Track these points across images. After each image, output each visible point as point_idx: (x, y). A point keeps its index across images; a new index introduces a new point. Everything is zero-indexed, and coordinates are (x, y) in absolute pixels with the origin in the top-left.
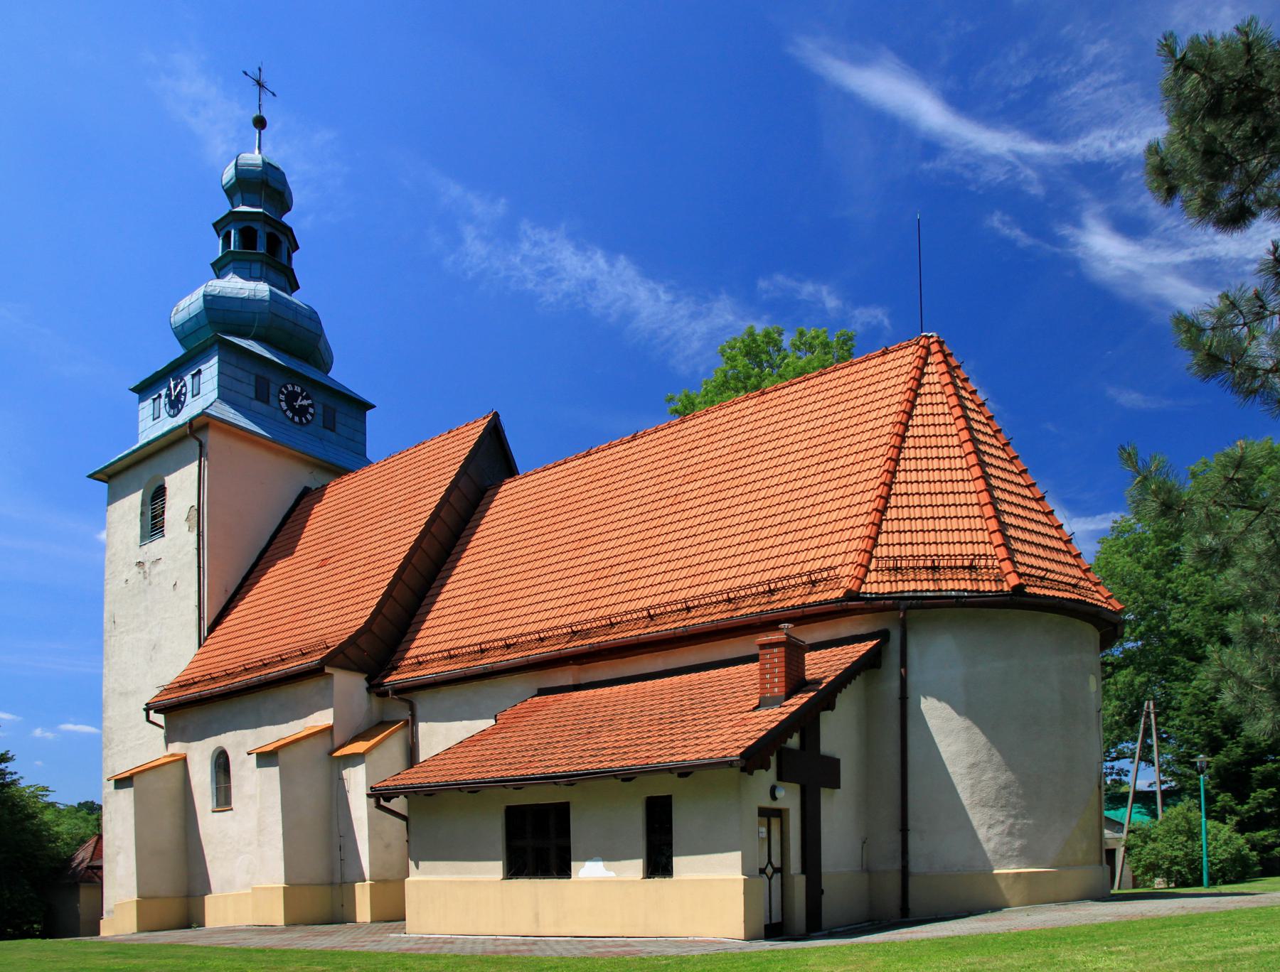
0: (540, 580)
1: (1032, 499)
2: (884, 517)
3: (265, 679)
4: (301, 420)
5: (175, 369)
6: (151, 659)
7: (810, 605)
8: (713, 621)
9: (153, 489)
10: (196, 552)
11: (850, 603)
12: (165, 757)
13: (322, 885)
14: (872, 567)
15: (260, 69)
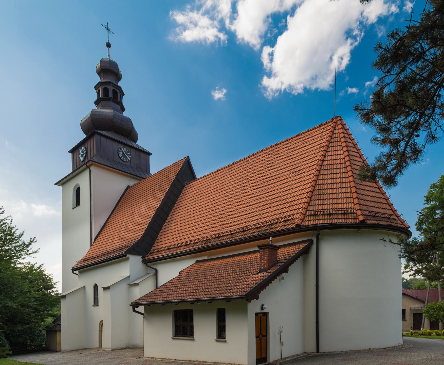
0: (199, 220)
2: (313, 194)
14: (307, 214)
15: (107, 23)
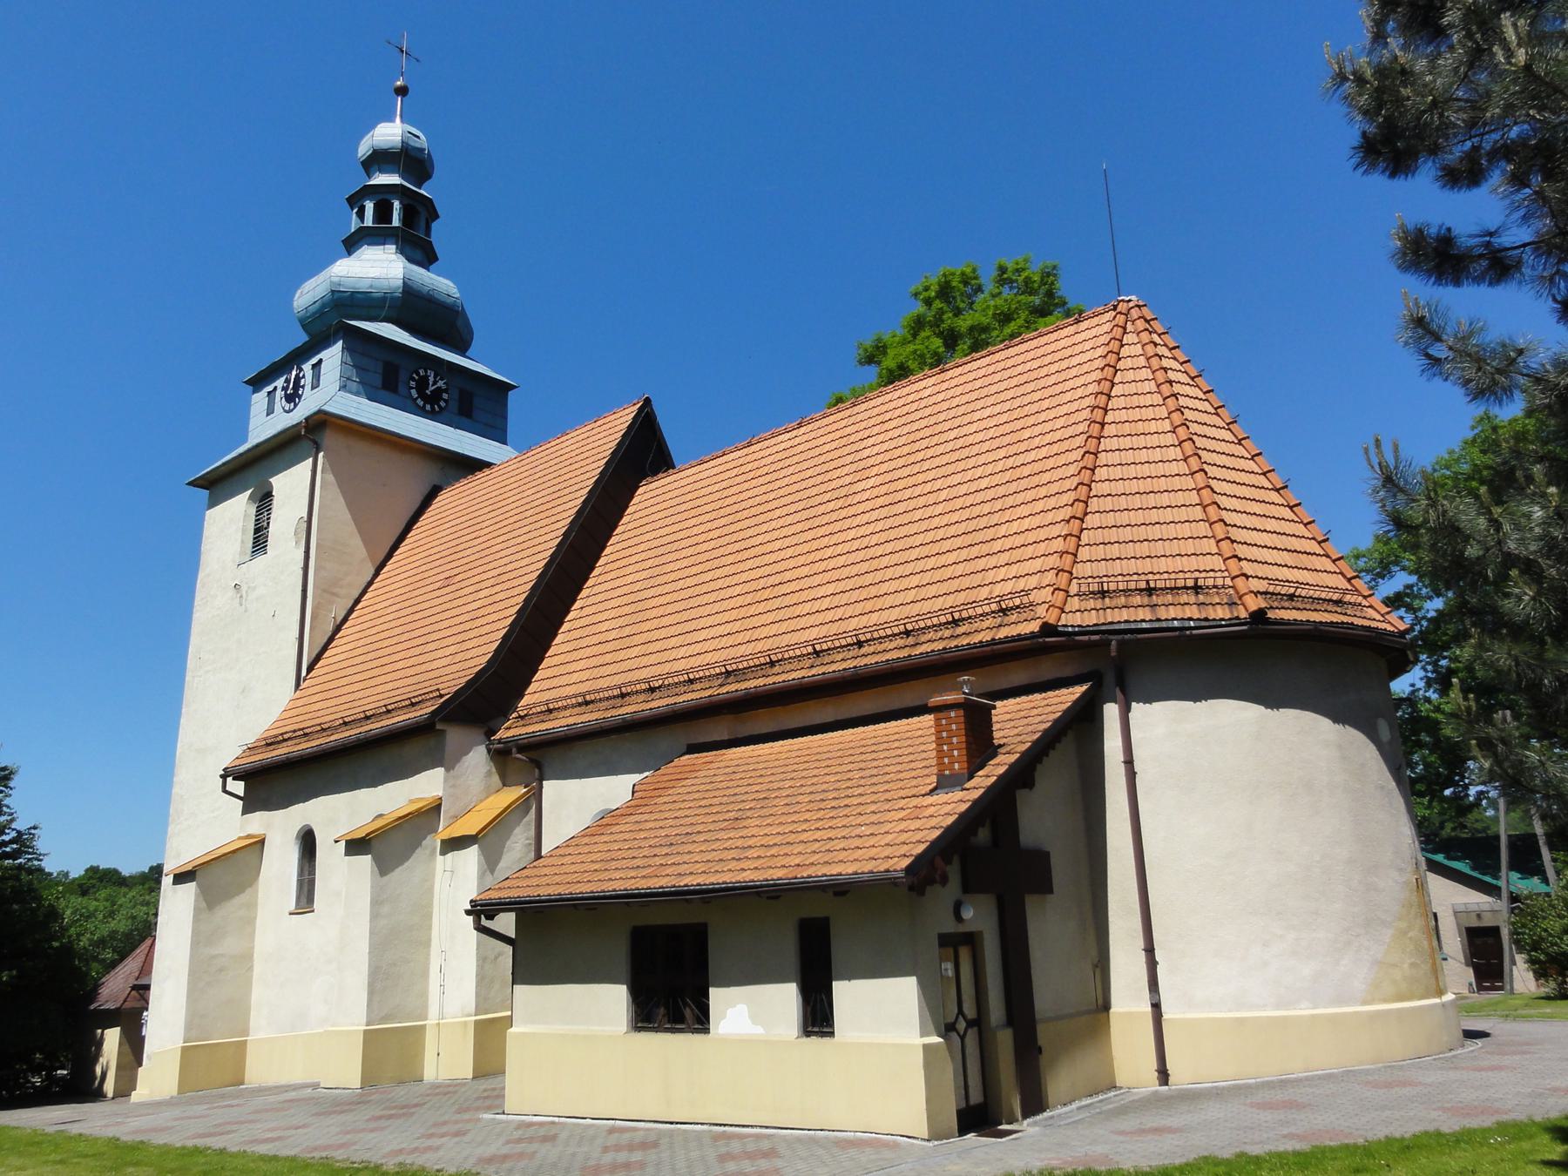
1: (1272, 489)
2: (1084, 526)
3: (366, 738)
4: (433, 408)
5: (297, 357)
7: (1001, 642)
8: (888, 660)
10: (301, 572)
11: (1047, 640)
12: (240, 838)
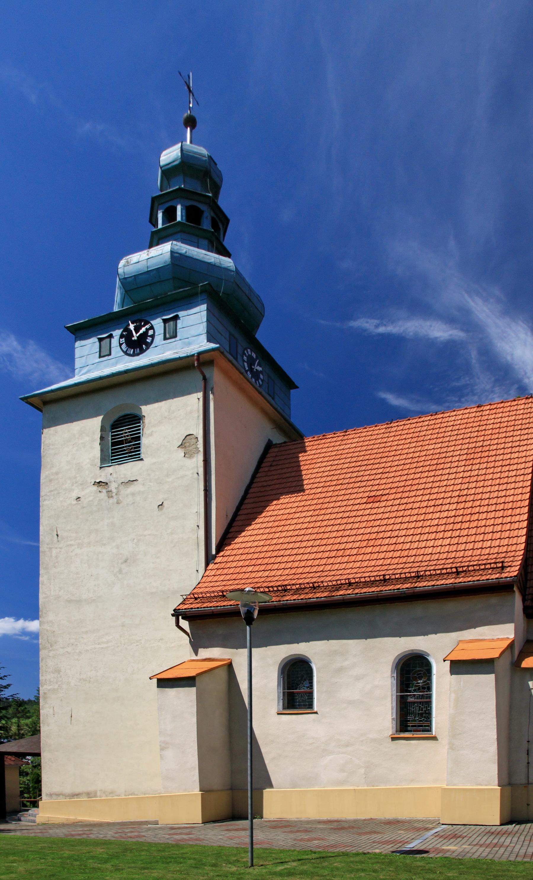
6: (120, 571)
9: (116, 417)
13: (227, 790)
